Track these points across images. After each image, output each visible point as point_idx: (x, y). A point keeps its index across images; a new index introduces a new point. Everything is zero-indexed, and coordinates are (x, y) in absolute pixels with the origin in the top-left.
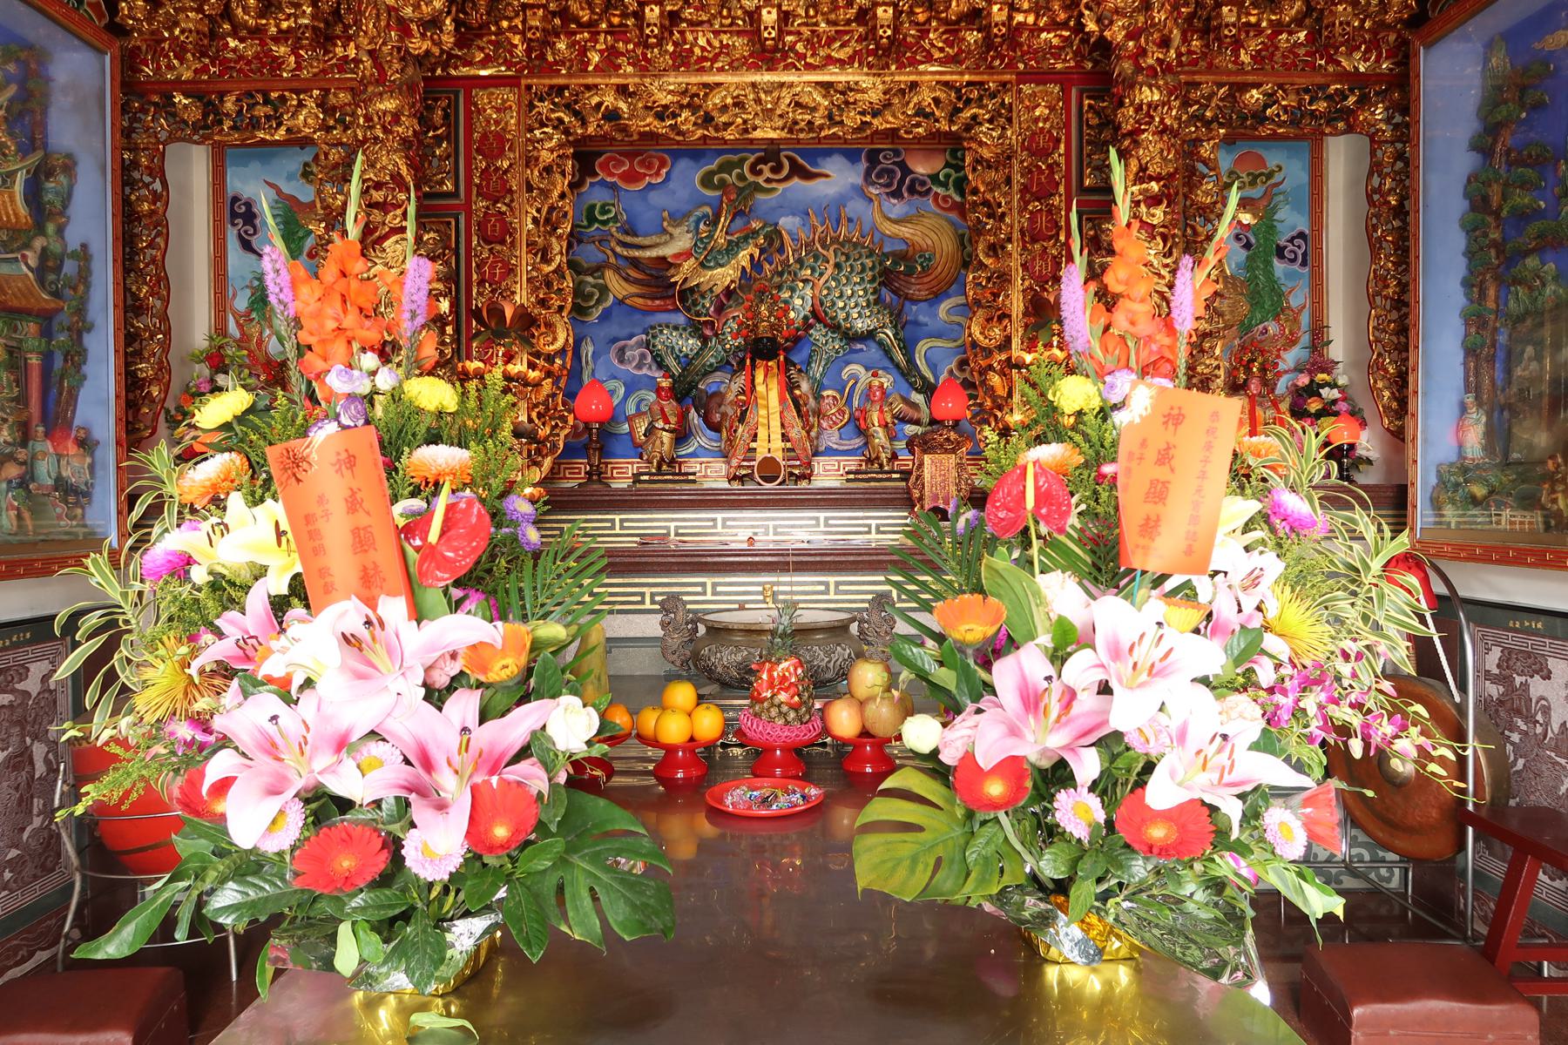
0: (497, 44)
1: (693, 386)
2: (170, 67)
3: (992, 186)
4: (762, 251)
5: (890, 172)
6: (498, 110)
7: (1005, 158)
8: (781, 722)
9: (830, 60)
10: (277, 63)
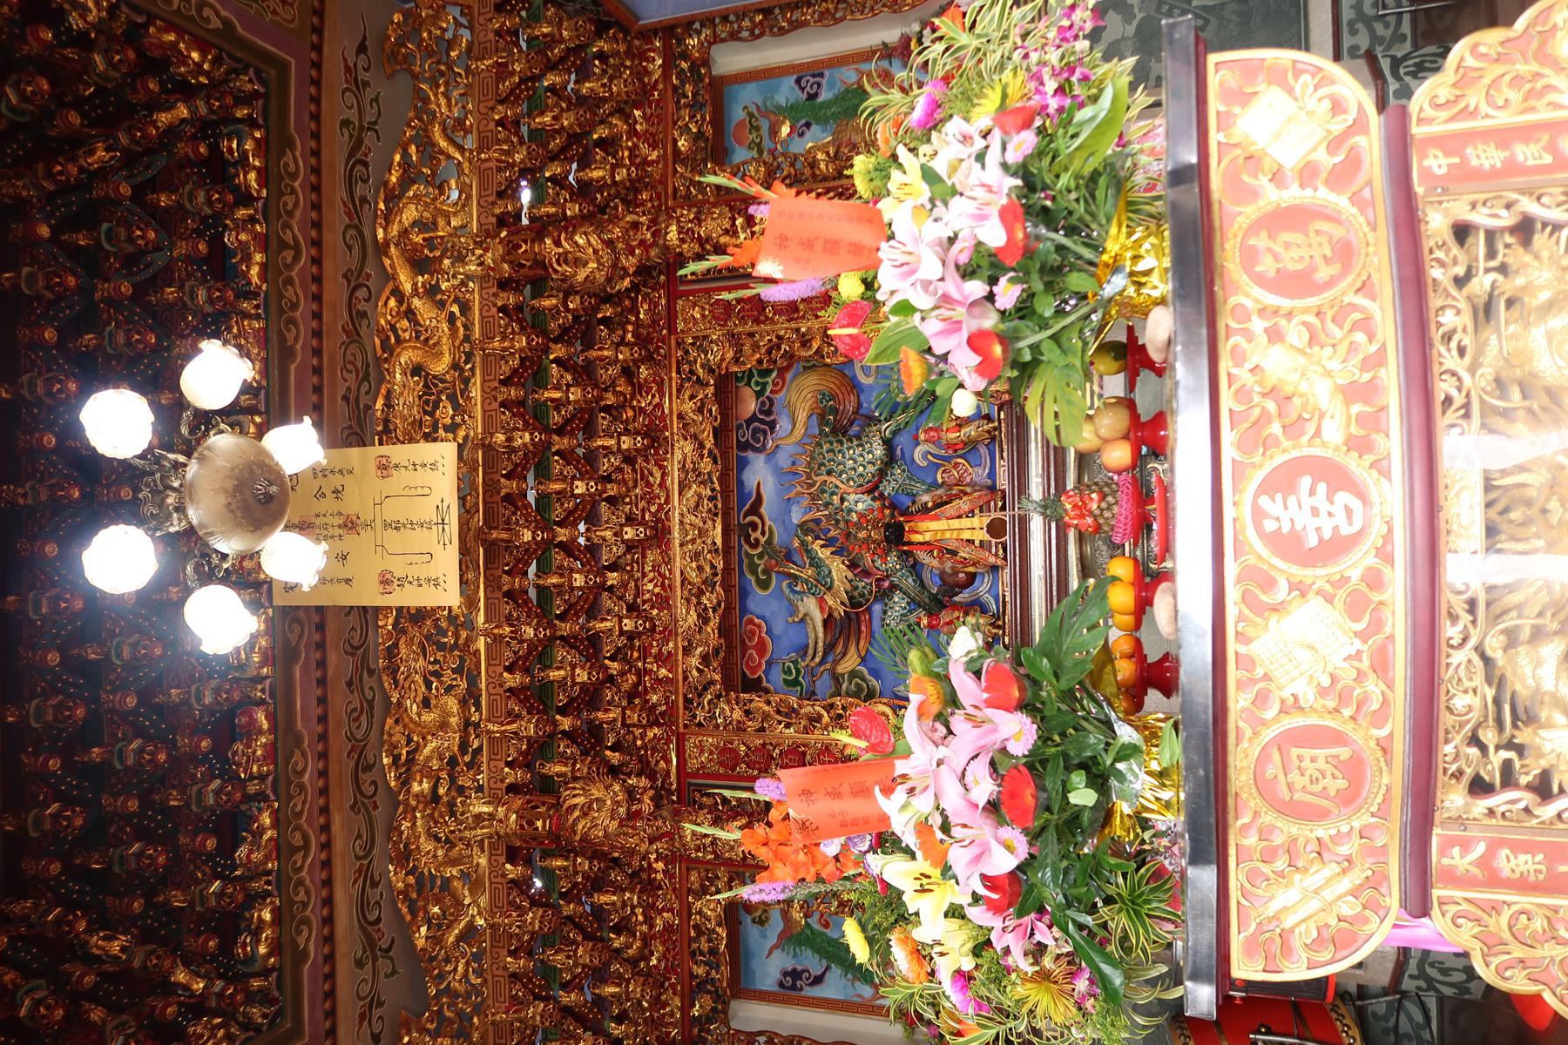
0: (654, 750)
1: (934, 598)
2: (672, 1014)
3: (756, 347)
4: (817, 538)
5: (755, 431)
6: (702, 751)
7: (734, 339)
8: (1116, 508)
9: (662, 485)
10: (668, 927)
